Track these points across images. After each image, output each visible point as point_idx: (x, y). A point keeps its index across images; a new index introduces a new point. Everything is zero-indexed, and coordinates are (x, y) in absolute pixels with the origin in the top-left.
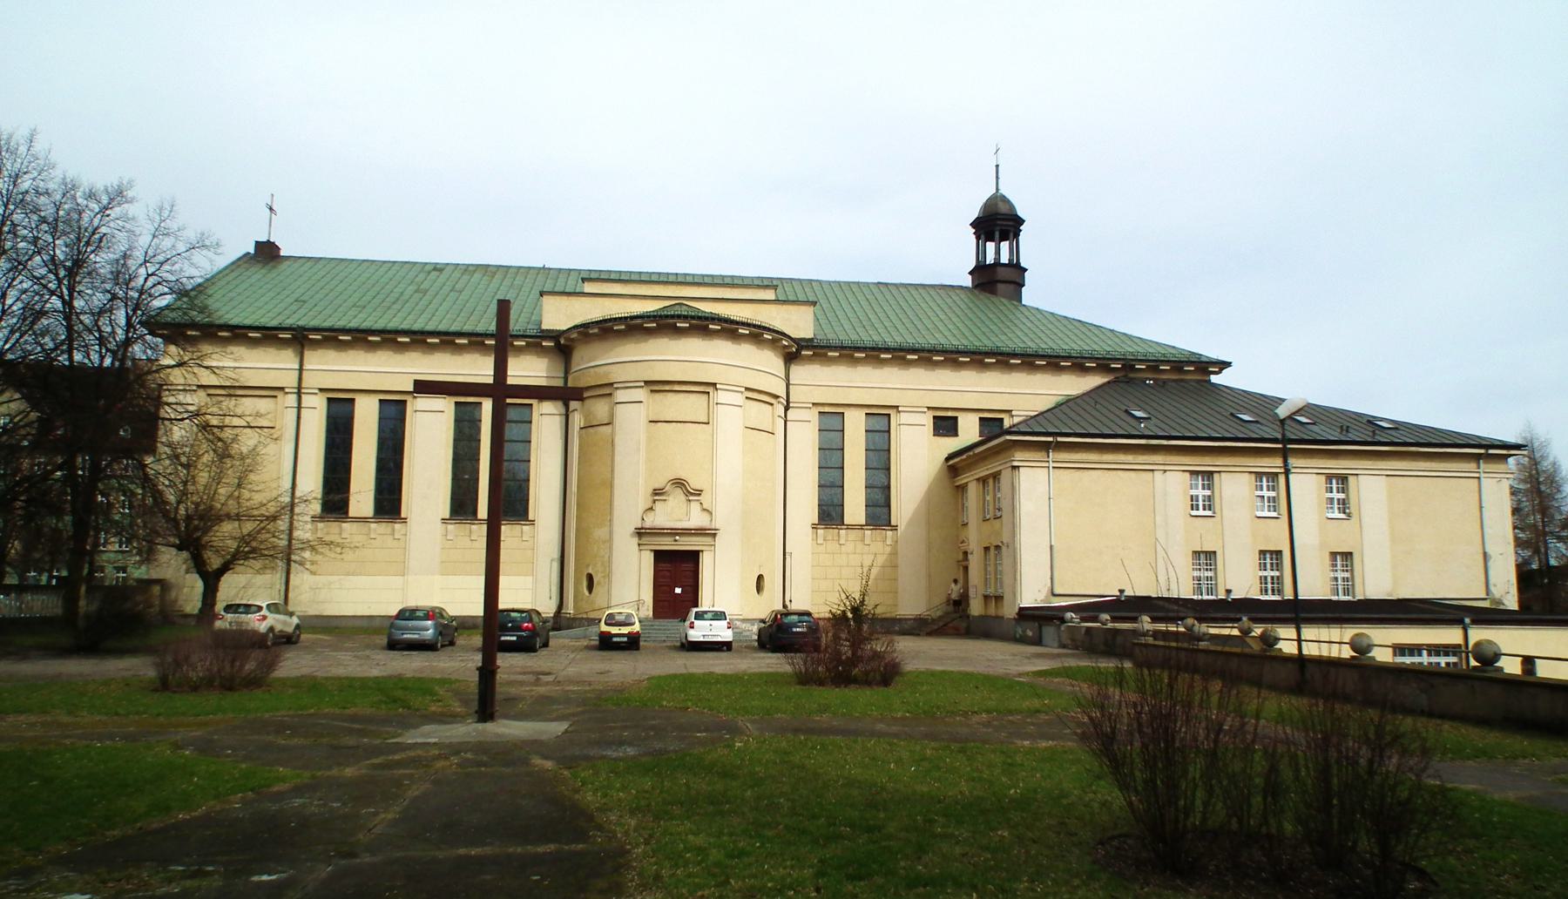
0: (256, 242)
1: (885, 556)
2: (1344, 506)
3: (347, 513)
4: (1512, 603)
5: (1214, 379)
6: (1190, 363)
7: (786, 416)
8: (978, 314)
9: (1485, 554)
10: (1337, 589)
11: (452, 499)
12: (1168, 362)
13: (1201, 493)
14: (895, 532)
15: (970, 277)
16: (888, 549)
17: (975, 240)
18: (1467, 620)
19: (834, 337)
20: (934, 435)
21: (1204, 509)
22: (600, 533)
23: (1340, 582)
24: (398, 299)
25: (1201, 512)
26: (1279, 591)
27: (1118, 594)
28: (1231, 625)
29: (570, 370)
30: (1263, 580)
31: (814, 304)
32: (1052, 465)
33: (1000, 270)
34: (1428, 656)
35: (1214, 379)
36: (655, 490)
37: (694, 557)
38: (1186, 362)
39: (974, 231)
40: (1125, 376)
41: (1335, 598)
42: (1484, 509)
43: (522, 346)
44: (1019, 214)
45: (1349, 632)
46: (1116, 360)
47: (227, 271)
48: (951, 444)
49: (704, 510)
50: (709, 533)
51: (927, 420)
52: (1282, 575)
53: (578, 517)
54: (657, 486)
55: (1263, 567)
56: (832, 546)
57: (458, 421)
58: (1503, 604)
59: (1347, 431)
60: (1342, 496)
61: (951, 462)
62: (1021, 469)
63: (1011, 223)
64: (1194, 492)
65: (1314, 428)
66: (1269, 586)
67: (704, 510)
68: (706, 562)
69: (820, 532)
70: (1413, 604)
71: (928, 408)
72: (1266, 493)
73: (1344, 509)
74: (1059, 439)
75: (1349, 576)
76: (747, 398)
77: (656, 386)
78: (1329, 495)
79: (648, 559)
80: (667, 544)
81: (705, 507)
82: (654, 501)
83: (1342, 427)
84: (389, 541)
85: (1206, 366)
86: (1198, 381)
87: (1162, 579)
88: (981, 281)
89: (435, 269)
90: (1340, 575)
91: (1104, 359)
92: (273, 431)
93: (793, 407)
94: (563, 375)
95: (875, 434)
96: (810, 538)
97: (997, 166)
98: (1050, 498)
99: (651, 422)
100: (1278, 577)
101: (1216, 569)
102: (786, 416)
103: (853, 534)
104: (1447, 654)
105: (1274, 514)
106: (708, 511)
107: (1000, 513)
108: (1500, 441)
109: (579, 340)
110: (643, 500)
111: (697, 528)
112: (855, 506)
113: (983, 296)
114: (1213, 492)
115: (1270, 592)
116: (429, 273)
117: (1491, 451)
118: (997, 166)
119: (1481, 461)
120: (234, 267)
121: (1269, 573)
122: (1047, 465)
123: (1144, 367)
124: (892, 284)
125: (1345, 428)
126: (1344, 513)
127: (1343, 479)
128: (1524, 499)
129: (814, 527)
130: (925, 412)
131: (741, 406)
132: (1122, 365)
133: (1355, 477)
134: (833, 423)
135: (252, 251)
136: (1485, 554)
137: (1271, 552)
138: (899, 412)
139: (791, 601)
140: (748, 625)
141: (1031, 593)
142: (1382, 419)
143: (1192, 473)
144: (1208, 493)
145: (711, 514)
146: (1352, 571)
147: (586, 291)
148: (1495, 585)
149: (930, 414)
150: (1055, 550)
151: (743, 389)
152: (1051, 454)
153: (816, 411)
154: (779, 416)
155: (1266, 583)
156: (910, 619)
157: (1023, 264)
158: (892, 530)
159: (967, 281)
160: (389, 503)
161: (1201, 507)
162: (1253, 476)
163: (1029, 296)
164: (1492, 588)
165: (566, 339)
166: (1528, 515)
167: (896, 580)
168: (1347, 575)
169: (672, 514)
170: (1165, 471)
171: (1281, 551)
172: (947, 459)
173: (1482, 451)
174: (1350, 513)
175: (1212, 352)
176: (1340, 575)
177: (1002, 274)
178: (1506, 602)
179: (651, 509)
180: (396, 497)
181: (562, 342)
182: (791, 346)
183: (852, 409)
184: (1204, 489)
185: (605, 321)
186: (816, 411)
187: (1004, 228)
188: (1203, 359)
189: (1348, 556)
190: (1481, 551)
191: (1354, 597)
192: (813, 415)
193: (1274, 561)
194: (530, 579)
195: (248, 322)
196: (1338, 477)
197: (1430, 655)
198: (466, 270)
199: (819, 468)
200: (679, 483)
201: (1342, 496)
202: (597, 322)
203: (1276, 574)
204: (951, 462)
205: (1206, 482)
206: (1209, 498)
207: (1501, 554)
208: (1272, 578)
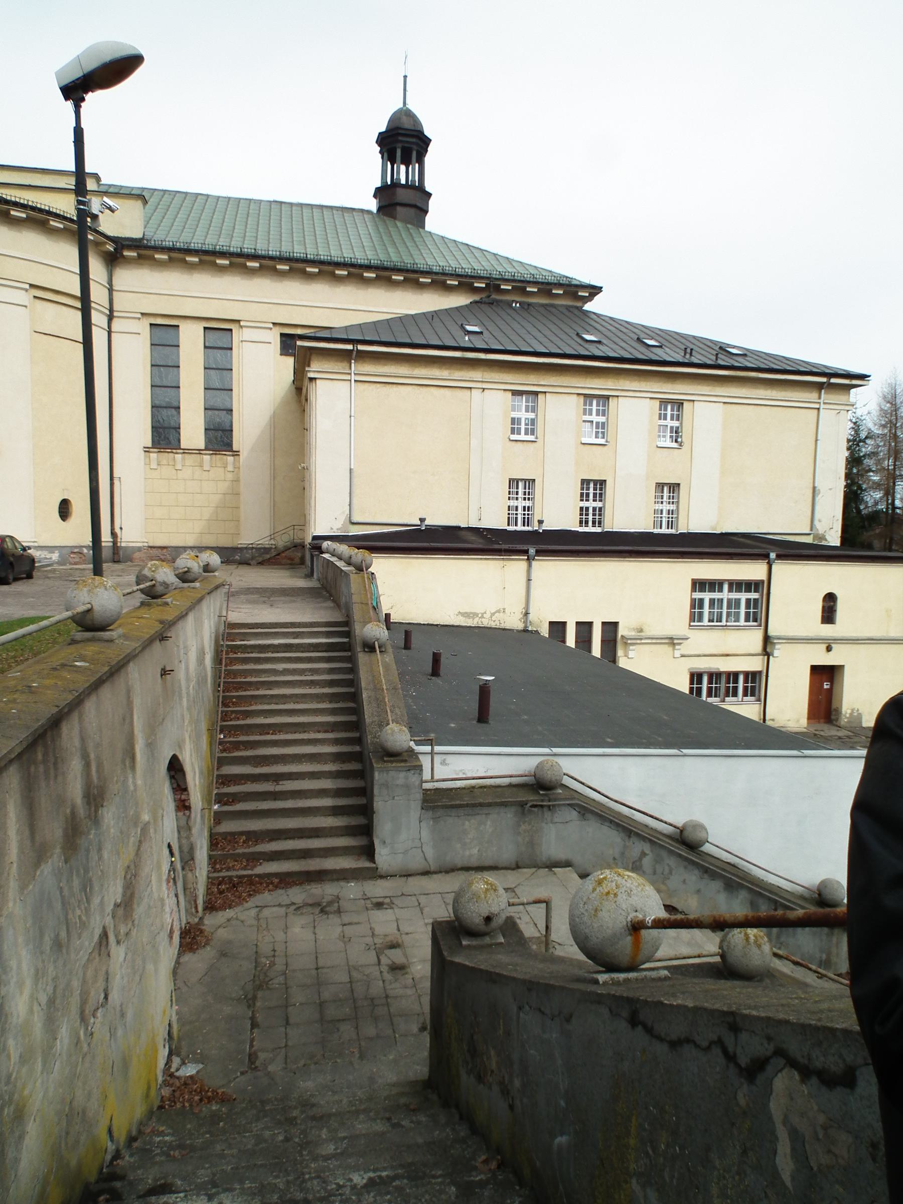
1: (227, 484)
2: (676, 434)
4: (834, 539)
5: (588, 307)
6: (559, 285)
7: (109, 327)
8: (384, 238)
9: (814, 488)
12: (535, 283)
13: (524, 415)
14: (237, 457)
16: (230, 476)
18: (773, 555)
20: (281, 355)
21: (526, 433)
25: (522, 437)
27: (419, 523)
32: (353, 377)
33: (399, 191)
35: (588, 307)
38: (555, 284)
40: (489, 296)
41: (512, 528)
42: (819, 442)
44: (426, 133)
46: (480, 278)
52: (604, 506)
55: (584, 497)
56: (167, 471)
58: (826, 540)
59: (691, 354)
60: (676, 424)
62: (318, 381)
63: (414, 140)
64: (515, 415)
65: (658, 351)
66: (590, 517)
69: (154, 456)
70: (735, 538)
71: (274, 324)
72: (595, 418)
73: (677, 437)
75: (675, 508)
76: (35, 297)
86: (568, 308)
87: (474, 508)
88: (384, 204)
90: (666, 507)
91: (466, 276)
93: (119, 317)
96: (143, 463)
97: (405, 77)
102: (109, 327)
103: (190, 459)
104: (748, 590)
108: (844, 370)
115: (590, 523)
117: (833, 380)
118: (405, 77)
119: (823, 391)
121: (591, 504)
122: (348, 377)
123: (510, 288)
125: (688, 351)
126: (676, 441)
127: (679, 404)
128: (881, 444)
129: (147, 450)
130: (271, 329)
131: (26, 307)
132: (486, 284)
133: (691, 403)
136: (814, 488)
137: (595, 482)
138: (241, 327)
139: (121, 528)
142: (734, 347)
143: (515, 393)
144: (531, 415)
148: (820, 521)
149: (277, 332)
150: (355, 474)
151: (27, 286)
152: (353, 365)
153: (147, 322)
155: (587, 515)
157: (428, 189)
158: (233, 455)
159: (372, 205)
163: (432, 223)
164: (816, 522)
166: (884, 459)
167: (238, 508)
170: (484, 389)
171: (605, 481)
173: (824, 380)
174: (682, 442)
176: (666, 507)
177: (402, 195)
178: (827, 537)
183: (188, 321)
184: (527, 411)
186: (147, 322)
187: (406, 145)
188: (574, 282)
190: (811, 486)
193: (598, 492)
196: (672, 402)
201: (676, 424)
206: (533, 422)
207: (830, 489)
208: (594, 509)
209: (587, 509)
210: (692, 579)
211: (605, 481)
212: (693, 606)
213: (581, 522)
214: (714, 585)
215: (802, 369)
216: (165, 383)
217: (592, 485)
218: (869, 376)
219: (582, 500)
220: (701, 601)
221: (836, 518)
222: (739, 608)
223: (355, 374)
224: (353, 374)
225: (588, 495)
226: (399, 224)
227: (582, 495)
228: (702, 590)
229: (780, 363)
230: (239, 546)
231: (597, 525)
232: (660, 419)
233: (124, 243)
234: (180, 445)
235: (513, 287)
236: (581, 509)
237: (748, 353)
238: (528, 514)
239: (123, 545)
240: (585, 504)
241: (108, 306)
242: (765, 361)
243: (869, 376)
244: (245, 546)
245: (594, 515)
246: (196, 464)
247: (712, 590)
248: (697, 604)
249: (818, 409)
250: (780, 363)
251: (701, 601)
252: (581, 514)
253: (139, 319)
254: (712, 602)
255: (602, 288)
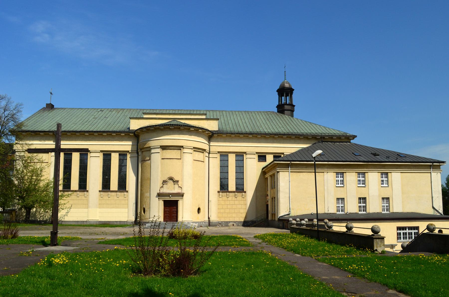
0: (47, 104)
3: (109, 189)
7: (209, 156)
10: (339, 210)
11: (102, 184)
15: (277, 108)
17: (278, 96)
19: (282, 131)
21: (341, 184)
22: (147, 195)
23: (385, 207)
24: (87, 121)
25: (340, 185)
26: (365, 210)
28: (172, 222)
29: (139, 142)
30: (360, 207)
31: (217, 119)
34: (408, 230)
36: (163, 181)
37: (176, 203)
39: (278, 93)
41: (338, 213)
42: (432, 183)
43: (123, 135)
45: (370, 225)
47: (37, 114)
48: (264, 164)
49: (179, 187)
50: (182, 195)
51: (256, 157)
53: (141, 190)
54: (164, 179)
55: (360, 203)
56: (225, 198)
57: (104, 160)
59: (389, 158)
61: (263, 170)
66: (362, 209)
67: (179, 187)
68: (180, 204)
74: (292, 162)
77: (164, 148)
78: (382, 179)
79: (162, 203)
80: (167, 199)
81: (179, 186)
82: (163, 184)
83: (387, 157)
84: (83, 198)
85: (348, 138)
89: (101, 111)
90: (340, 205)
92: (48, 163)
94: (136, 144)
95: (239, 161)
98: (289, 182)
99: (162, 159)
100: (365, 206)
101: (344, 204)
102: (209, 156)
103: (113, 194)
104: (414, 230)
105: (342, 185)
106: (181, 187)
107: (275, 186)
108: (438, 160)
109: (141, 133)
110: (160, 184)
111: (177, 193)
112: (232, 186)
113: (280, 114)
114: (344, 179)
115: (362, 211)
116: (99, 112)
120: (39, 112)
121: (362, 205)
122: (288, 171)
124: (275, 112)
125: (388, 157)
134: (240, 158)
135: (45, 107)
137: (363, 198)
140: (195, 224)
141: (282, 212)
144: (342, 179)
145: (182, 188)
146: (344, 204)
147: (144, 117)
153: (102, 153)
154: (206, 156)
155: (361, 208)
156: (250, 221)
159: (276, 110)
160: (83, 186)
161: (340, 184)
162: (357, 174)
165: (137, 133)
168: (343, 205)
169: (170, 189)
170: (327, 172)
171: (366, 198)
172: (263, 169)
175: (351, 132)
176: (385, 205)
179: (162, 187)
180: (85, 184)
181: (136, 133)
182: (210, 133)
185: (148, 127)
189: (388, 199)
191: (390, 212)
192: (218, 156)
193: (364, 201)
194: (127, 209)
195: (40, 130)
197: (409, 230)
198: (110, 111)
199: (220, 172)
200: (171, 179)
202: (145, 127)
203: (364, 205)
204: (263, 170)
205: (386, 176)
207: (438, 197)
209: (361, 206)
210: (397, 227)
211: (366, 198)
212: (398, 235)
213: (359, 210)
214: (404, 228)
215: (424, 161)
216: (224, 172)
217: (362, 199)
218: (446, 162)
219: (359, 204)
220: (400, 233)
221: (440, 206)
222: (407, 235)
223: (290, 170)
224: (290, 170)
225: (361, 202)
226: (287, 116)
227: (359, 202)
228: (400, 230)
229: (417, 159)
230: (246, 221)
231: (364, 211)
232: (381, 178)
233: (214, 132)
234: (228, 190)
235: (329, 137)
236: (359, 206)
237: (407, 156)
238: (343, 209)
239: (211, 221)
240: (360, 205)
241: (209, 150)
242: (412, 159)
243: (446, 162)
244: (250, 221)
245: (363, 208)
246: (233, 196)
247: (403, 230)
248: (399, 234)
249: (431, 173)
250: (417, 159)
251: (400, 233)
252: (359, 208)
253: (217, 153)
254: (403, 233)
255: (357, 136)
